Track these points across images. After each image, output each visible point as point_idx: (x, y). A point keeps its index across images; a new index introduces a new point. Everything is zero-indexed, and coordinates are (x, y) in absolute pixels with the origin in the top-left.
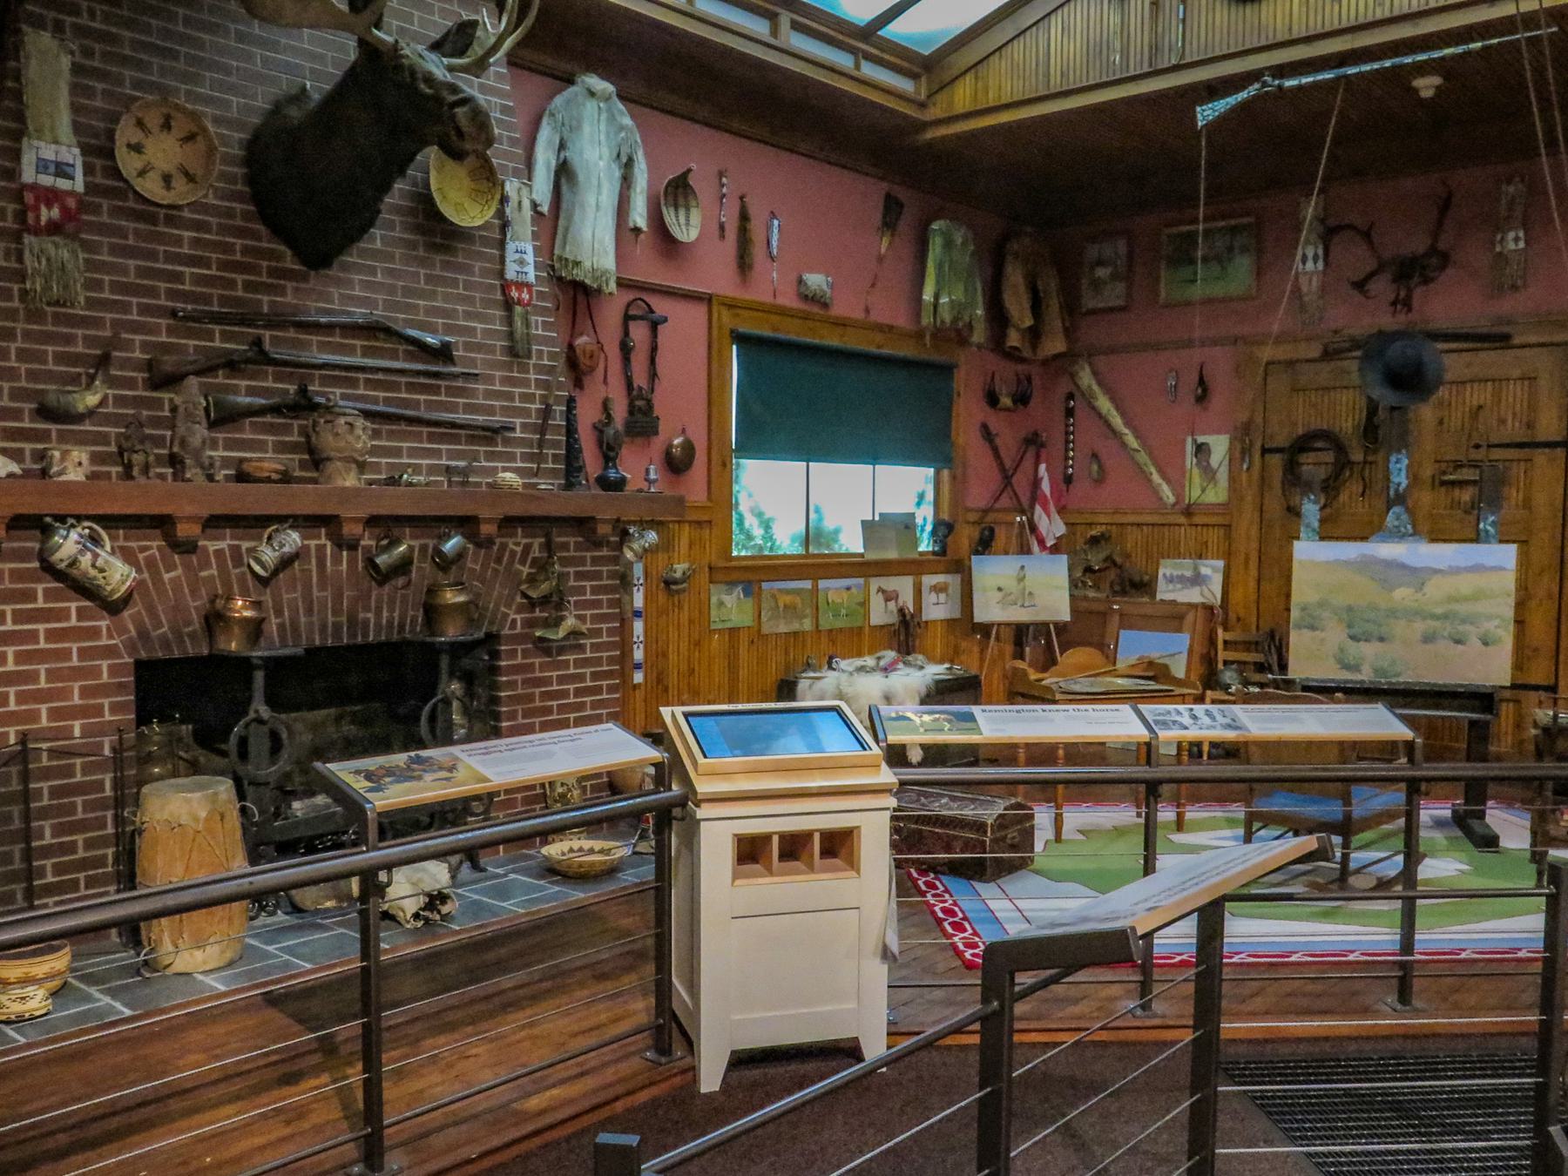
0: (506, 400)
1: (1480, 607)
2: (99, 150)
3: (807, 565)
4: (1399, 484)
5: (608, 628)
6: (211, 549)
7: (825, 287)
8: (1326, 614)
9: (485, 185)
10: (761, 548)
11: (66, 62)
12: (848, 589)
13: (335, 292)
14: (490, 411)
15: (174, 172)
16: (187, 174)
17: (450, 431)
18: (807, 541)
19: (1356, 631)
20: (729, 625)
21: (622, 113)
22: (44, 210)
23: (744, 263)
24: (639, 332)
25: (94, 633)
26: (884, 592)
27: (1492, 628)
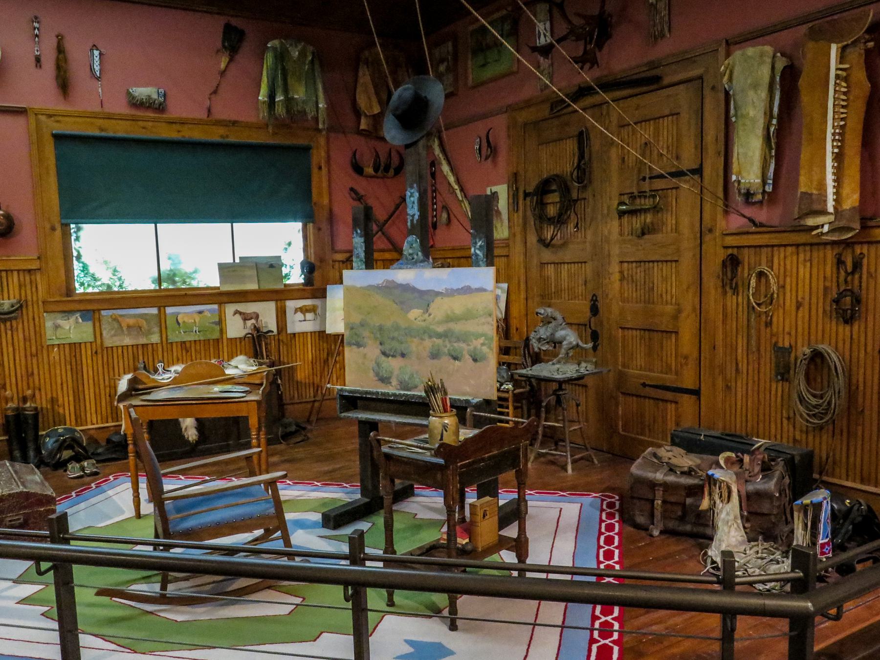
1: (470, 327)
4: (413, 216)
7: (155, 96)
8: (366, 333)
12: (200, 312)
18: (159, 280)
19: (387, 347)
23: (64, 85)
27: (479, 347)
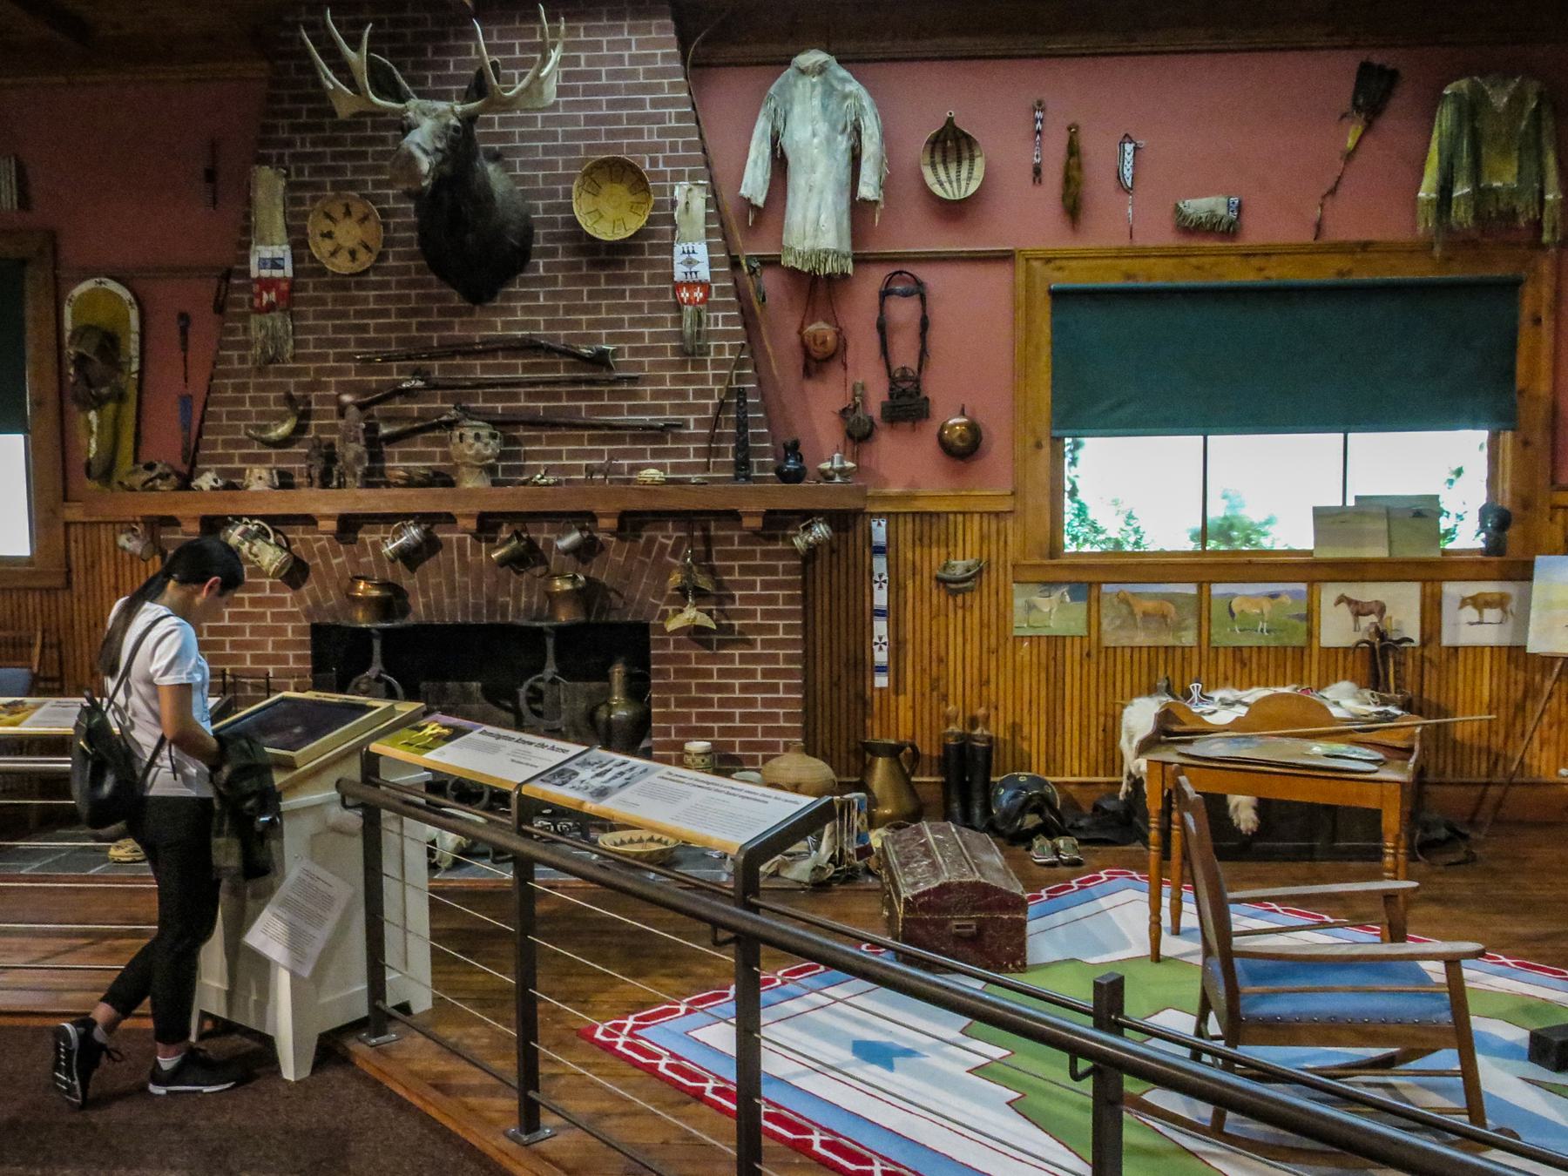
0: (678, 398)
2: (299, 245)
3: (1201, 564)
5: (785, 625)
6: (368, 541)
9: (641, 197)
10: (1118, 543)
11: (282, 183)
12: (1273, 596)
13: (499, 321)
14: (660, 410)
15: (357, 247)
16: (367, 247)
17: (613, 433)
20: (1045, 632)
21: (843, 81)
22: (265, 296)
23: (1073, 208)
24: (903, 311)
25: (282, 602)
26: (1350, 602)
